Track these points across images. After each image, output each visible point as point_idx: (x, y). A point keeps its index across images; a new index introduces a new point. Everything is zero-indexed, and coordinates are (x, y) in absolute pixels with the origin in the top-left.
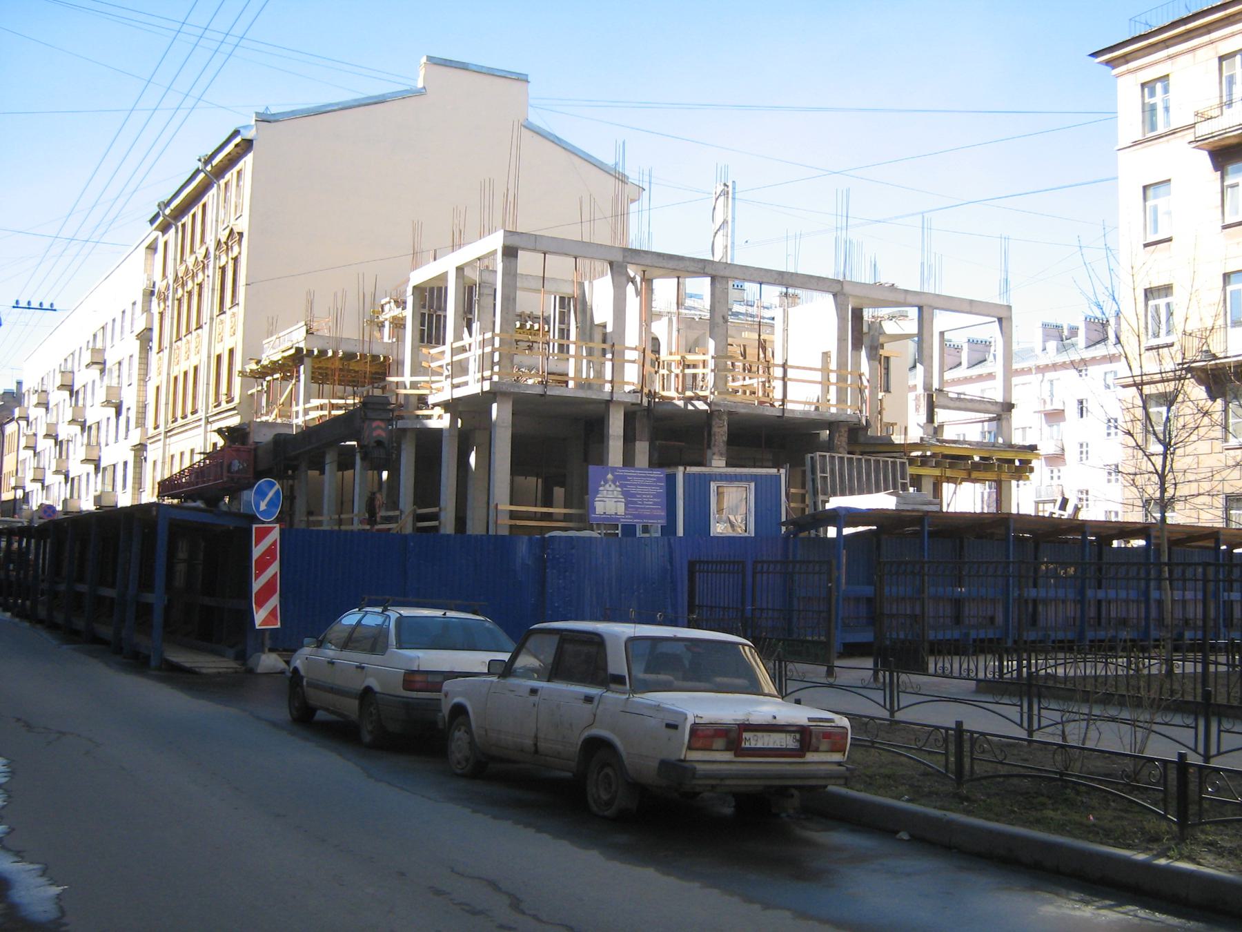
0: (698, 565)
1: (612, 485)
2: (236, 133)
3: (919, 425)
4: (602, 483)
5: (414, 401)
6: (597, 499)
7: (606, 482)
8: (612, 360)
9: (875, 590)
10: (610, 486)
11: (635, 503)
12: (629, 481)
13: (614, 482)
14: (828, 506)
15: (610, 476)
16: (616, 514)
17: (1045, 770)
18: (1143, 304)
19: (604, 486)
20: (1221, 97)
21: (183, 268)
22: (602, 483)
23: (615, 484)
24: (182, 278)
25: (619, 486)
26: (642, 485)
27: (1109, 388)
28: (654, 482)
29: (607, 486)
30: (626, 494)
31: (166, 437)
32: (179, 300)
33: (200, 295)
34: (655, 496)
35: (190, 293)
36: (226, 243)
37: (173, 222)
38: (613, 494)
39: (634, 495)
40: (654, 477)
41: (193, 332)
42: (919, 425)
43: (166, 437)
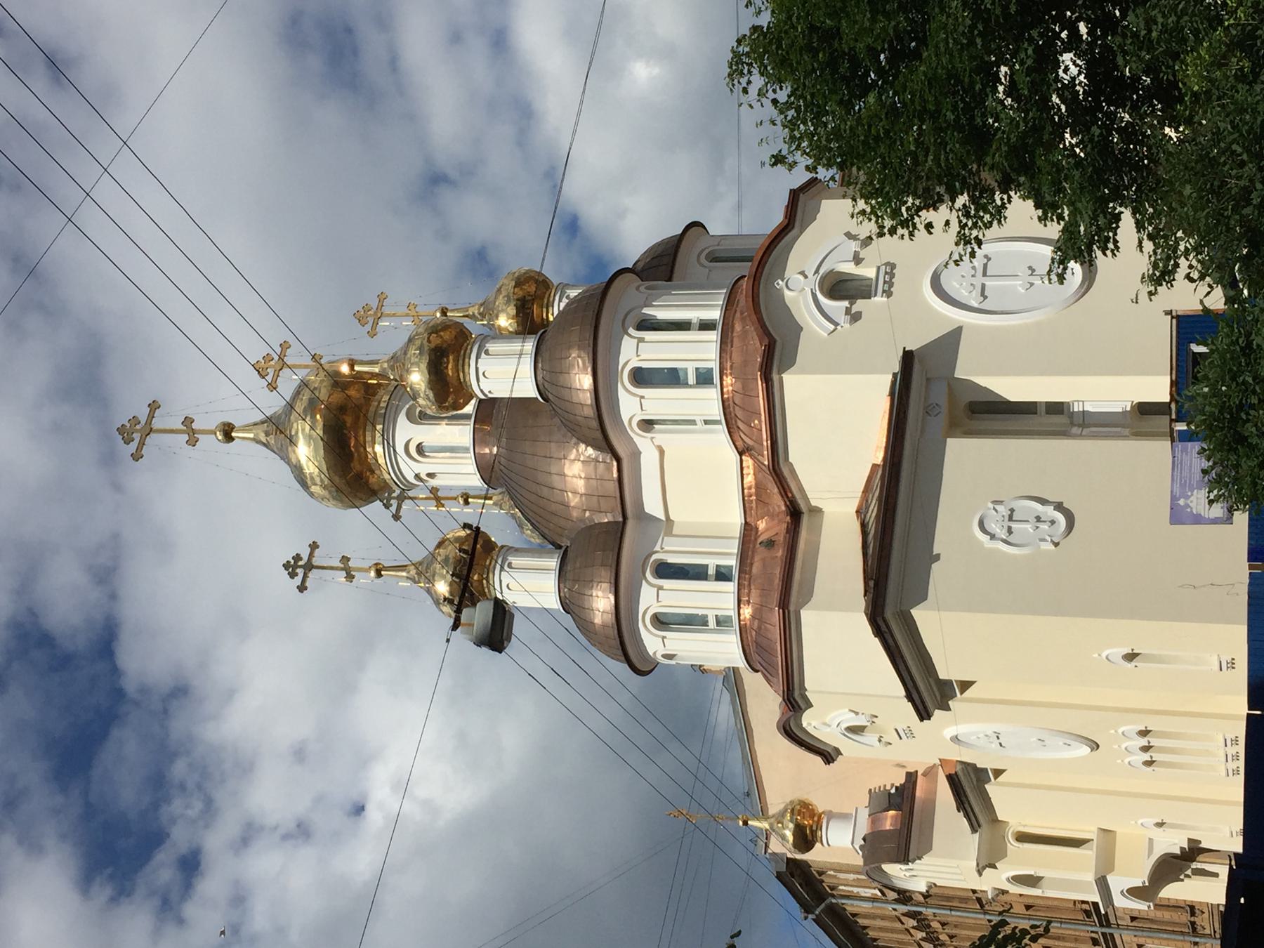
0: (1005, 101)
1: (1191, 499)
3: (904, 348)
4: (1189, 510)
5: (1222, 405)
6: (1207, 516)
7: (1187, 506)
10: (1191, 502)
12: (1185, 481)
13: (1187, 497)
14: (643, 311)
15: (1182, 502)
17: (908, 823)
18: (477, 384)
19: (1192, 508)
22: (1189, 510)
23: (1190, 497)
25: (1192, 492)
26: (1191, 467)
27: (775, 124)
28: (1187, 454)
31: (1109, 925)
35: (951, 937)
38: (1201, 498)
40: (1182, 456)
42: (904, 348)
43: (1109, 925)
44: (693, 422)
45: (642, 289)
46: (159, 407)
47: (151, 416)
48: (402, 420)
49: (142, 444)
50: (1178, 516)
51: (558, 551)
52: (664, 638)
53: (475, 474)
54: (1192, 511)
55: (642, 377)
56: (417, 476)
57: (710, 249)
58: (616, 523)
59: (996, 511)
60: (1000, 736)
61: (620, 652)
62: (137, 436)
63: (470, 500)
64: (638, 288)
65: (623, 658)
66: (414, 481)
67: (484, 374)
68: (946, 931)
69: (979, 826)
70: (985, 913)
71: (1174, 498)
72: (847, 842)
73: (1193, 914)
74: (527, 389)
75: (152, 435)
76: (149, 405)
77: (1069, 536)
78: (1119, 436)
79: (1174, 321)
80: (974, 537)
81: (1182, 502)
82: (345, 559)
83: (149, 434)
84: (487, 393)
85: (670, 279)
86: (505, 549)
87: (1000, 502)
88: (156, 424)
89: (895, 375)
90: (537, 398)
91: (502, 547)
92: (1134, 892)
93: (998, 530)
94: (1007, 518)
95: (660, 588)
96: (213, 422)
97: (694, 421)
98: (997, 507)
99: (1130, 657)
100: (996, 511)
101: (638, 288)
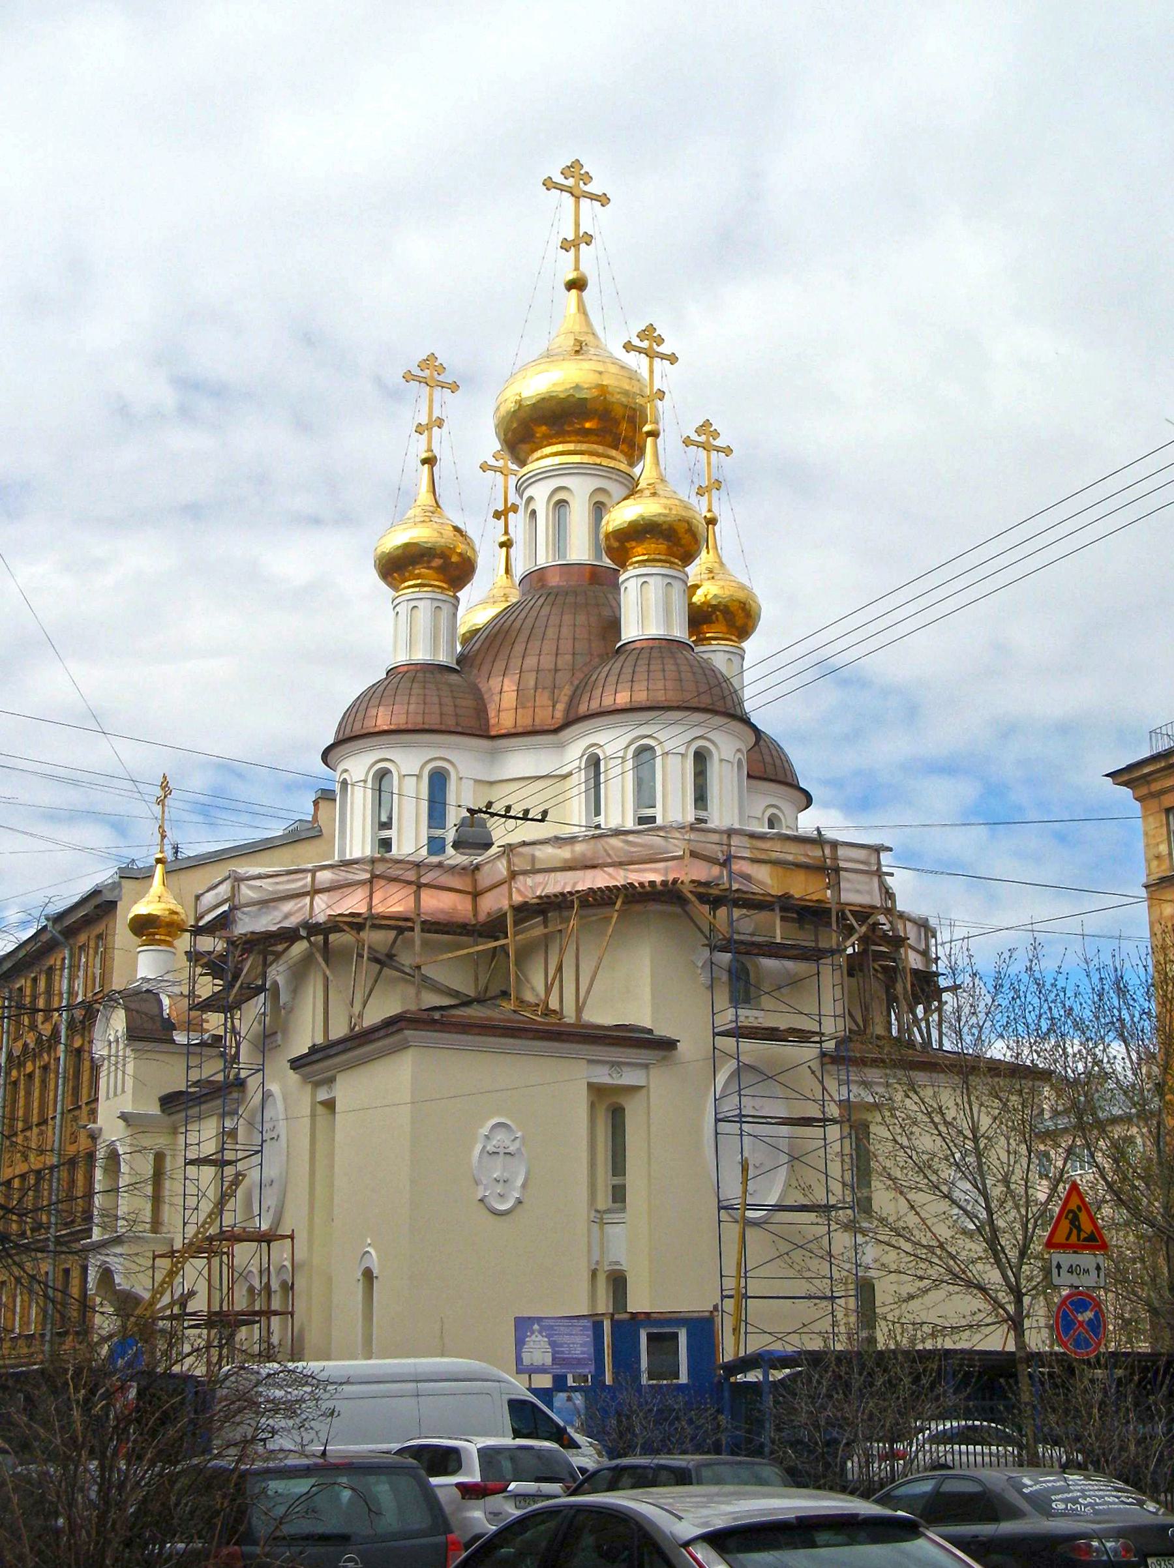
2: (594, 1274)
3: (678, 1041)
7: (532, 1333)
8: (240, 1019)
9: (618, 833)
11: (562, 1352)
13: (540, 1332)
15: (536, 1327)
16: (543, 1365)
20: (845, 860)
21: (20, 1044)
24: (18, 1057)
29: (534, 1336)
30: (553, 1344)
32: (15, 1083)
33: (44, 1082)
34: (582, 1345)
35: (30, 1076)
36: (82, 1022)
37: (766, 1389)
39: (561, 1345)
41: (34, 1128)
42: (678, 1041)
44: (597, 813)
45: (739, 755)
46: (602, 205)
47: (593, 197)
48: (593, 483)
49: (561, 188)
50: (523, 1326)
51: (455, 662)
52: (365, 781)
53: (536, 565)
54: (528, 1336)
55: (644, 754)
56: (531, 499)
57: (782, 818)
58: (488, 729)
59: (514, 1140)
60: (274, 1141)
61: (348, 734)
62: (570, 182)
63: (504, 549)
64: (739, 750)
65: (341, 737)
66: (526, 496)
67: (645, 582)
68: (37, 1071)
69: (169, 1114)
70: (62, 1113)
71: (539, 1320)
72: (142, 972)
73: (77, 1333)
74: (630, 631)
75: (572, 199)
76: (605, 195)
77: (488, 1212)
78: (328, 799)
79: (707, 1314)
80: (489, 1119)
81: (536, 1327)
82: (440, 423)
83: (573, 195)
84: (625, 585)
85: (749, 776)
86: (456, 603)
87: (523, 1144)
88: (585, 203)
89: (650, 1031)
90: (620, 640)
91: (457, 599)
92: (106, 1275)
93: (494, 1142)
94: (506, 1151)
95: (418, 776)
96: (587, 268)
97: (599, 815)
98: (518, 1140)
99: (368, 1275)
100: (514, 1140)
101: (739, 750)
